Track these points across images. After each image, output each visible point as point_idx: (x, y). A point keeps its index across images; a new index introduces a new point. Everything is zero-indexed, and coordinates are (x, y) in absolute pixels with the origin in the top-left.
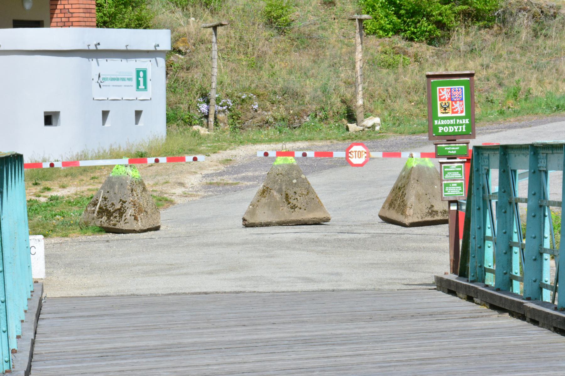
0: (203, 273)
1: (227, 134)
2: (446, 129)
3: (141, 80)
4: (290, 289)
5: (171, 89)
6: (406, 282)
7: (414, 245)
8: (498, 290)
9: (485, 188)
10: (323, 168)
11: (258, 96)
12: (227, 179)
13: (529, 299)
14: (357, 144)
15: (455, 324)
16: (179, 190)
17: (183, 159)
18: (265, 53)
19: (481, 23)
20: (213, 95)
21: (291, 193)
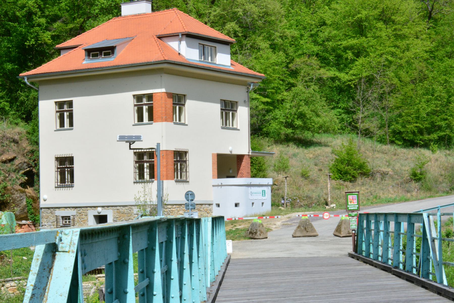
0: (279, 251)
1: (290, 209)
2: (351, 208)
3: (264, 193)
4: (304, 256)
5: (273, 196)
6: (340, 254)
7: (343, 243)
8: (366, 257)
9: (362, 226)
10: (317, 220)
11: (299, 198)
12: (289, 223)
13: (374, 260)
14: (326, 213)
15: (352, 267)
16: (274, 226)
17: (274, 217)
18: (301, 185)
19: (366, 176)
20: (285, 198)
21: (307, 227)
